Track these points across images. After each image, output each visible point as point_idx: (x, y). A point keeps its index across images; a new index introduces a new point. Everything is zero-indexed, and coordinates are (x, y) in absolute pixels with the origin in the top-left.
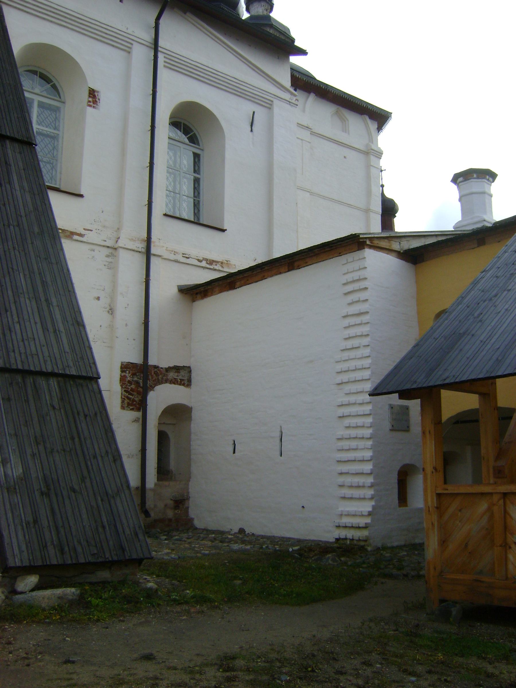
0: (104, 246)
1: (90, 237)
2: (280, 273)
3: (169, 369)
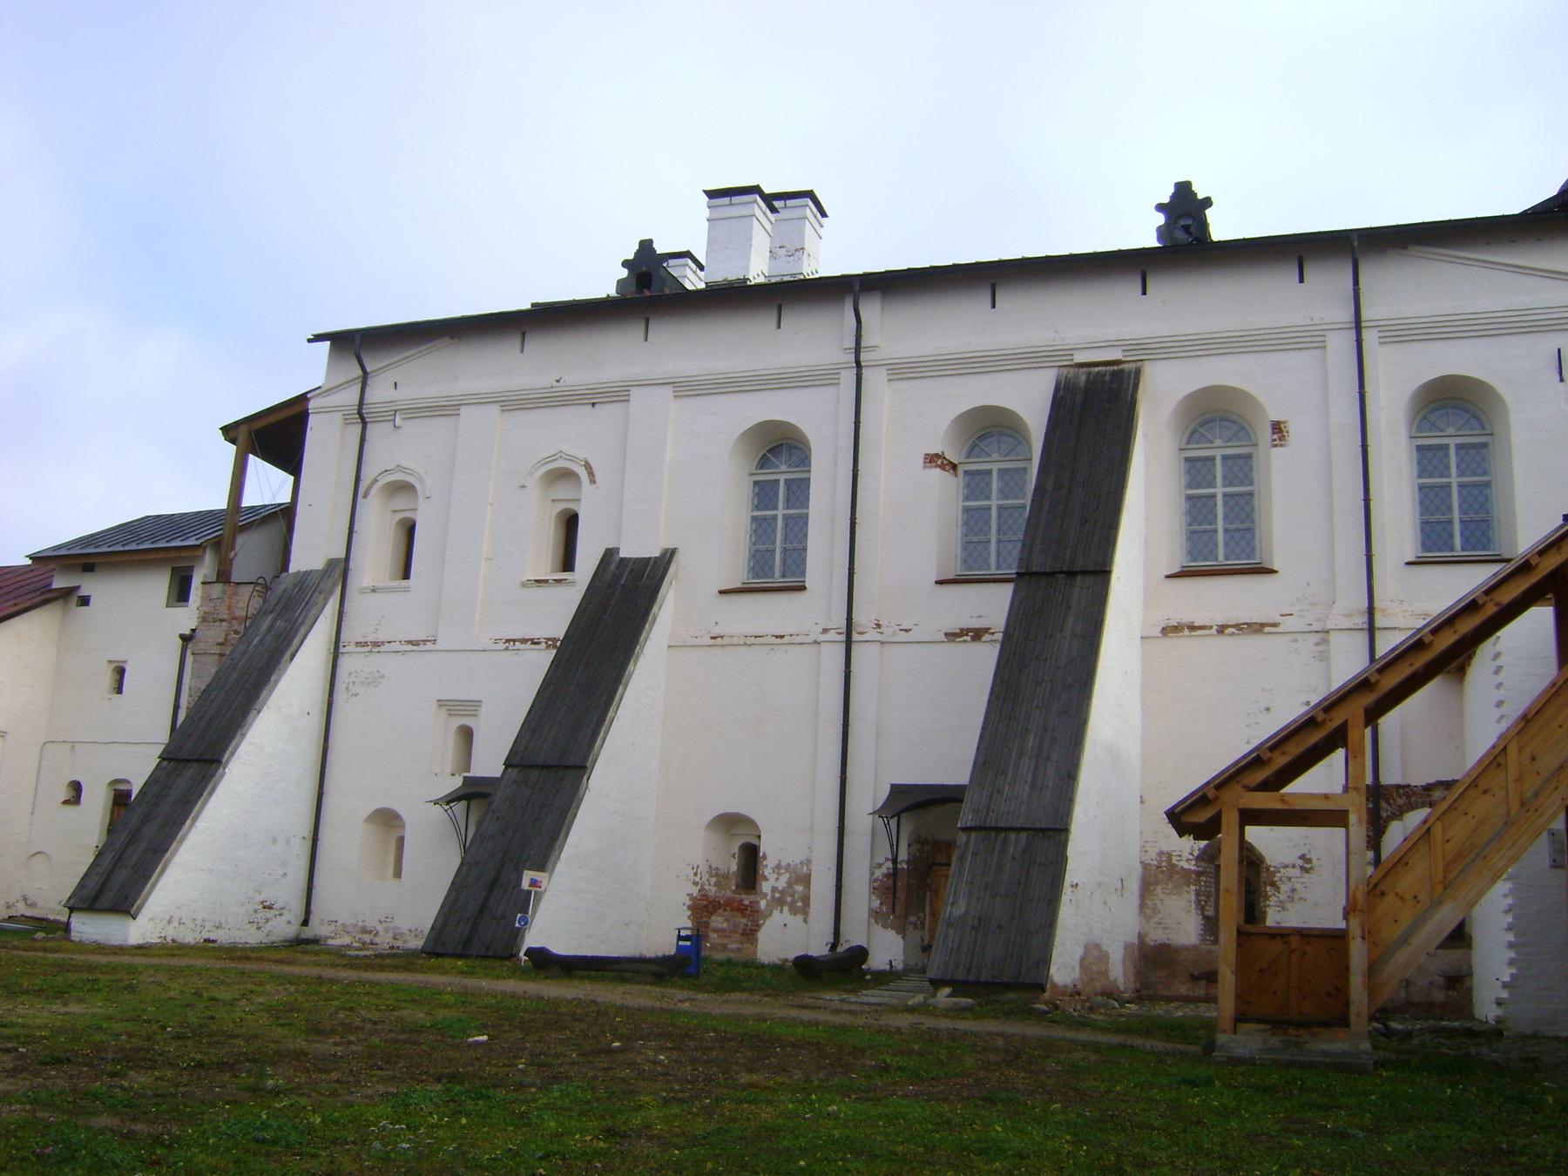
1: (1288, 624)
3: (1428, 788)
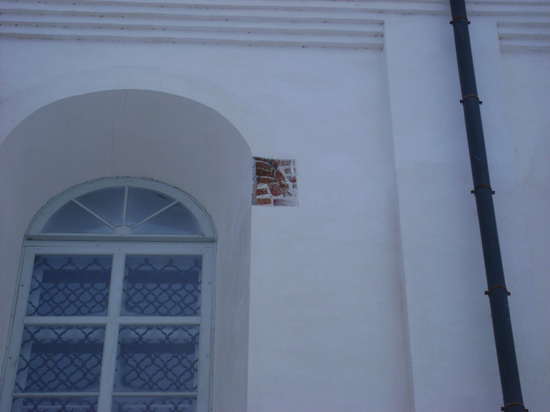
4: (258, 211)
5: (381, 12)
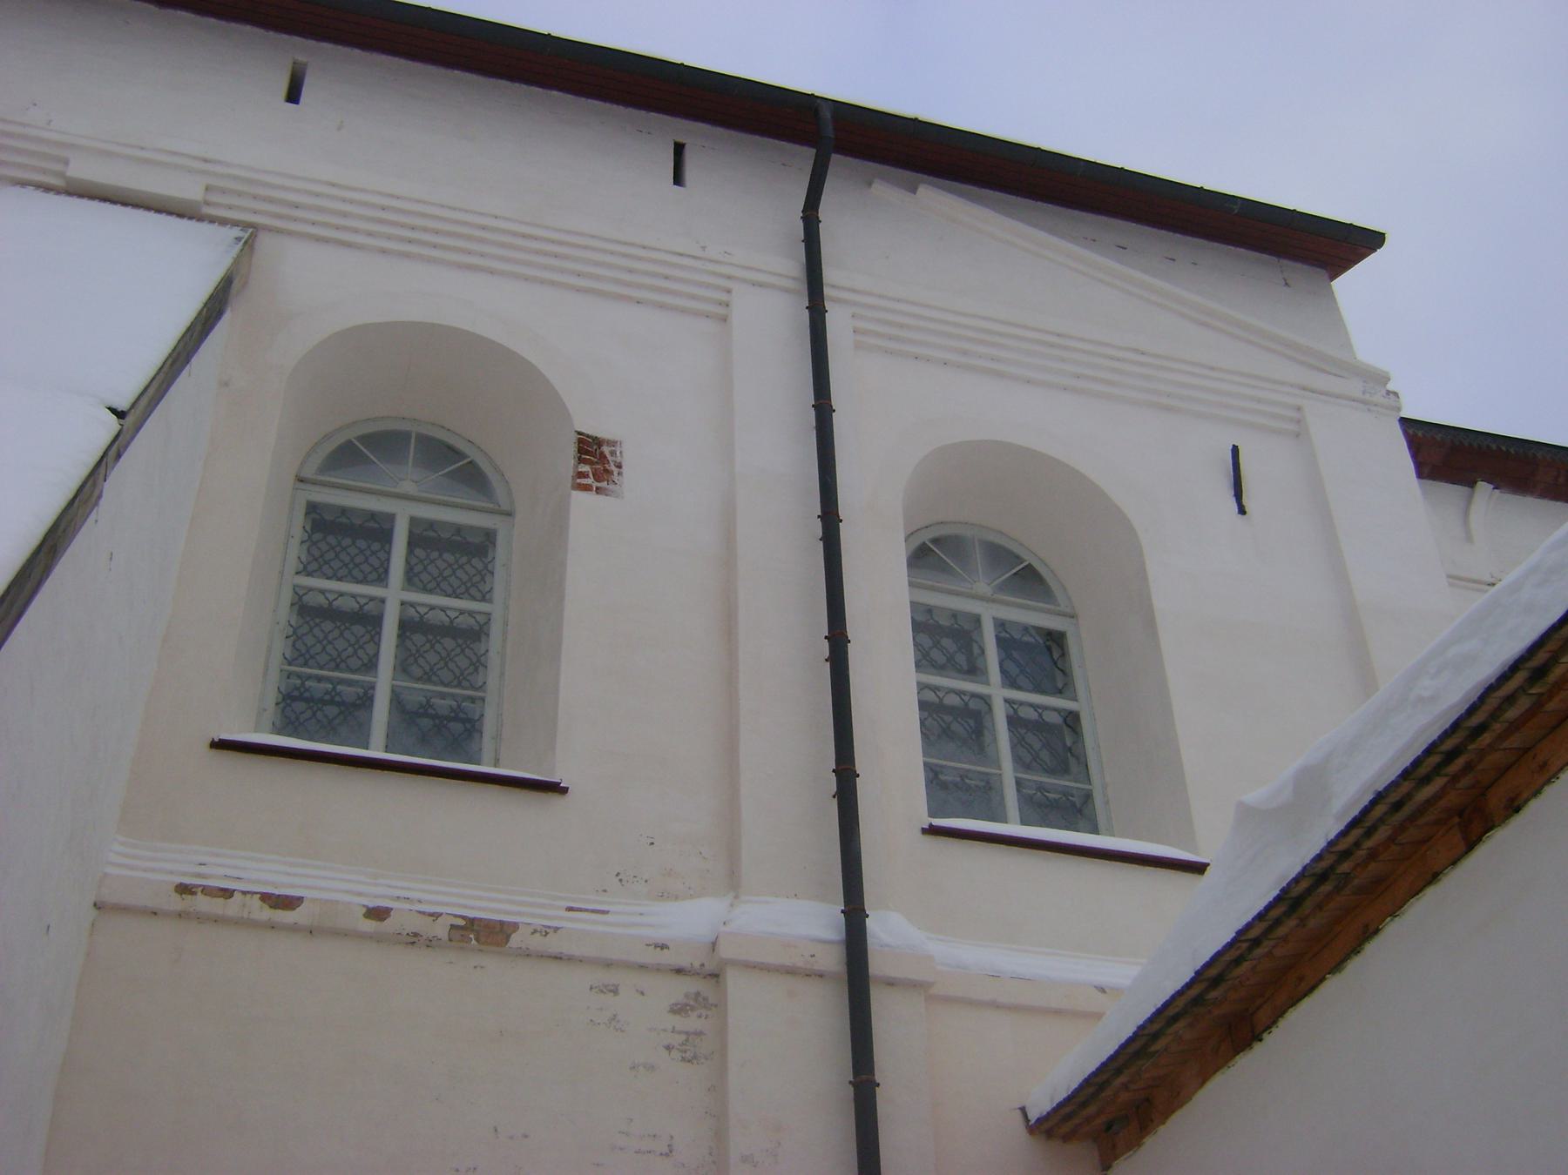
0: (659, 969)
2: (1434, 877)
4: (579, 497)
5: (729, 277)
